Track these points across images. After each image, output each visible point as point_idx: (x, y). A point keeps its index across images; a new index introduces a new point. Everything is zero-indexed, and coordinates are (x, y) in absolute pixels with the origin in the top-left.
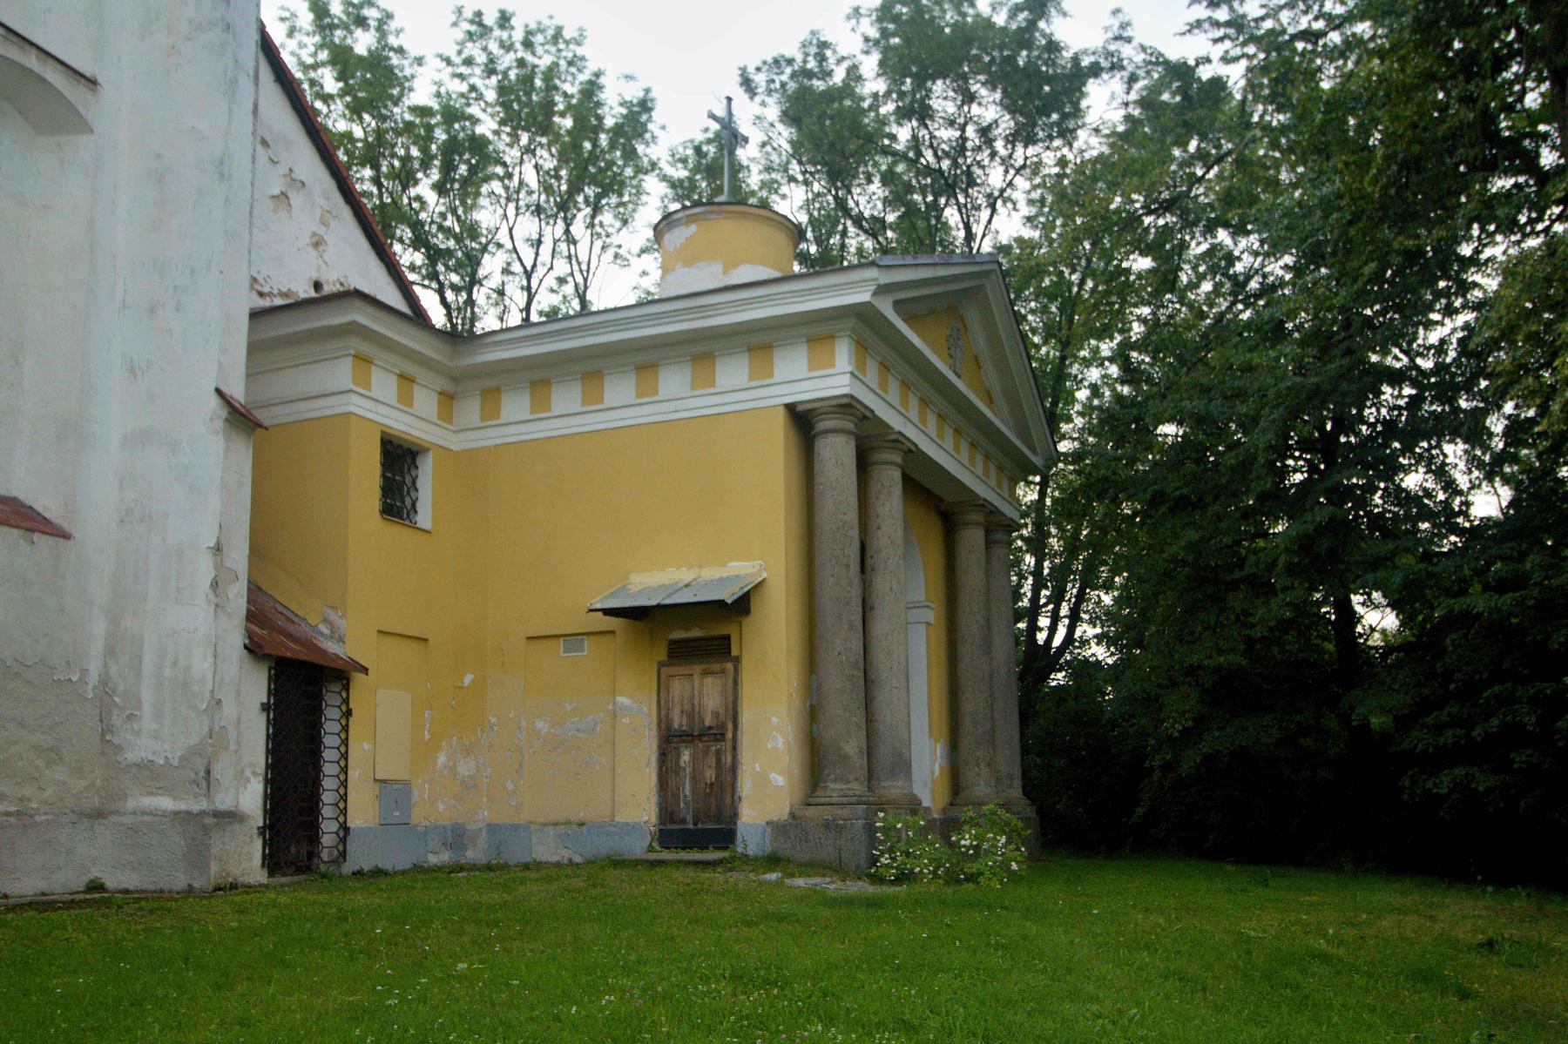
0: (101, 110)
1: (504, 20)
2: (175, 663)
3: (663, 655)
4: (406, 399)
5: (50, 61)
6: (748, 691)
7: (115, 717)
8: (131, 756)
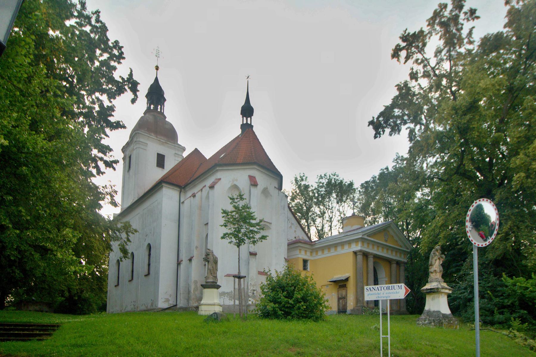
1: (325, 175)
3: (338, 287)
4: (306, 254)
6: (348, 292)
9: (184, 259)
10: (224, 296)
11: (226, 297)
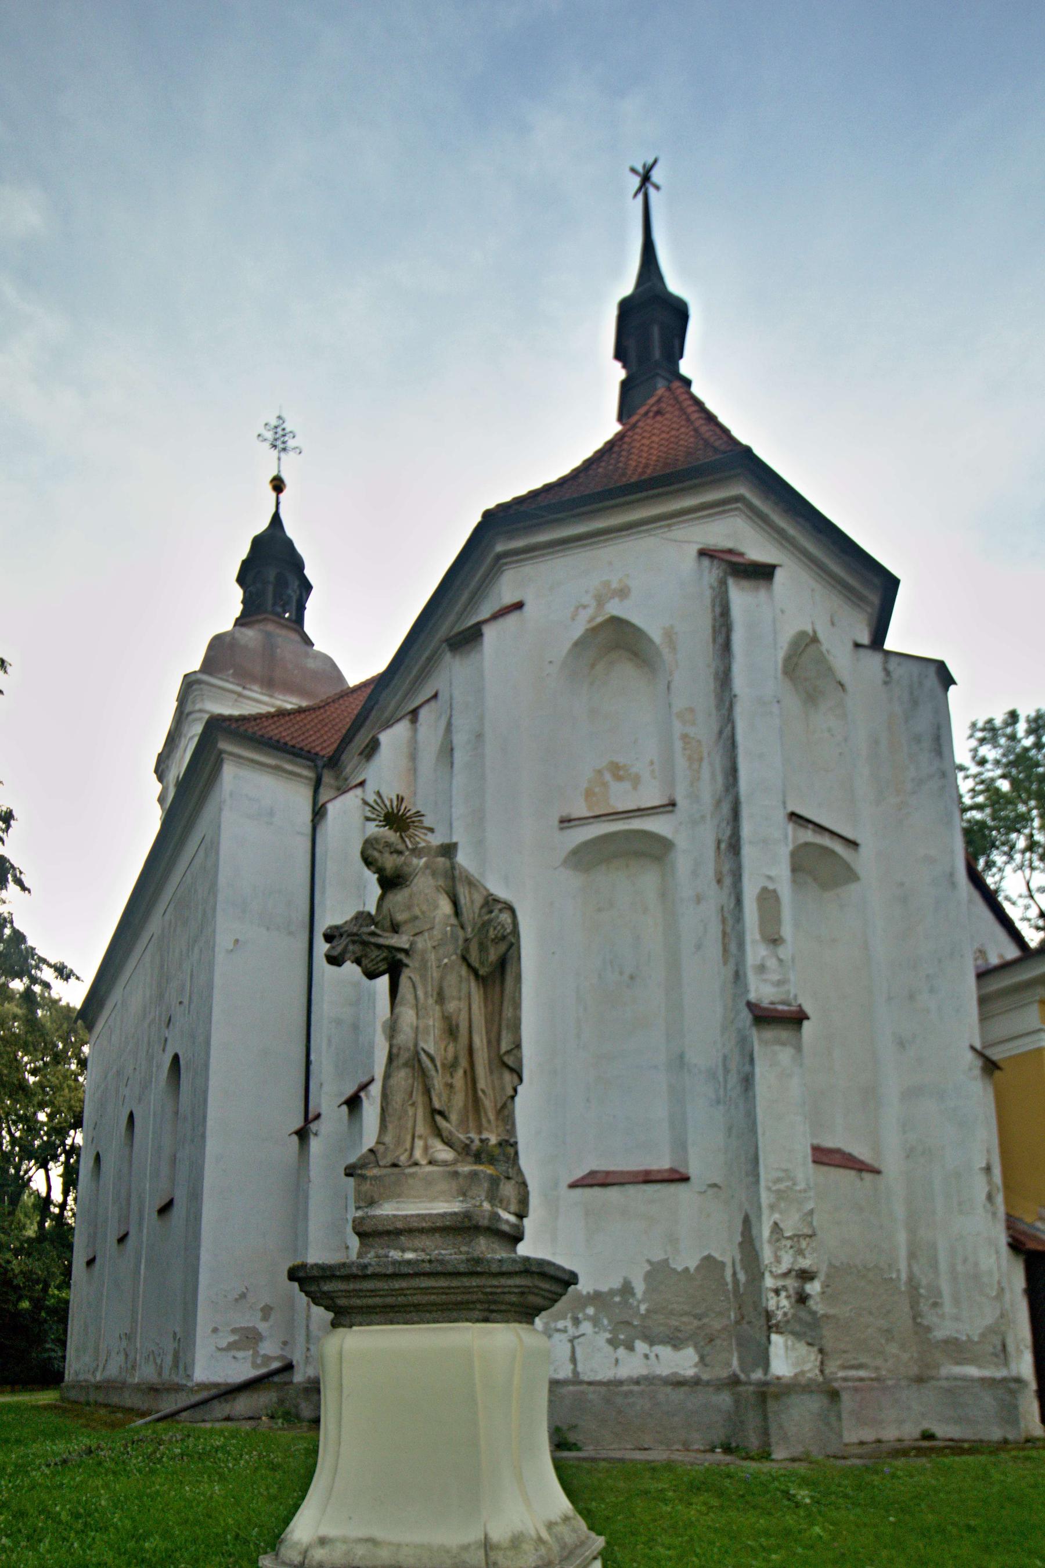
0: (865, 861)
2: (965, 1260)
5: (835, 837)
7: (922, 1305)
8: (939, 1334)
9: (324, 1110)
10: (576, 1322)
11: (586, 1327)
